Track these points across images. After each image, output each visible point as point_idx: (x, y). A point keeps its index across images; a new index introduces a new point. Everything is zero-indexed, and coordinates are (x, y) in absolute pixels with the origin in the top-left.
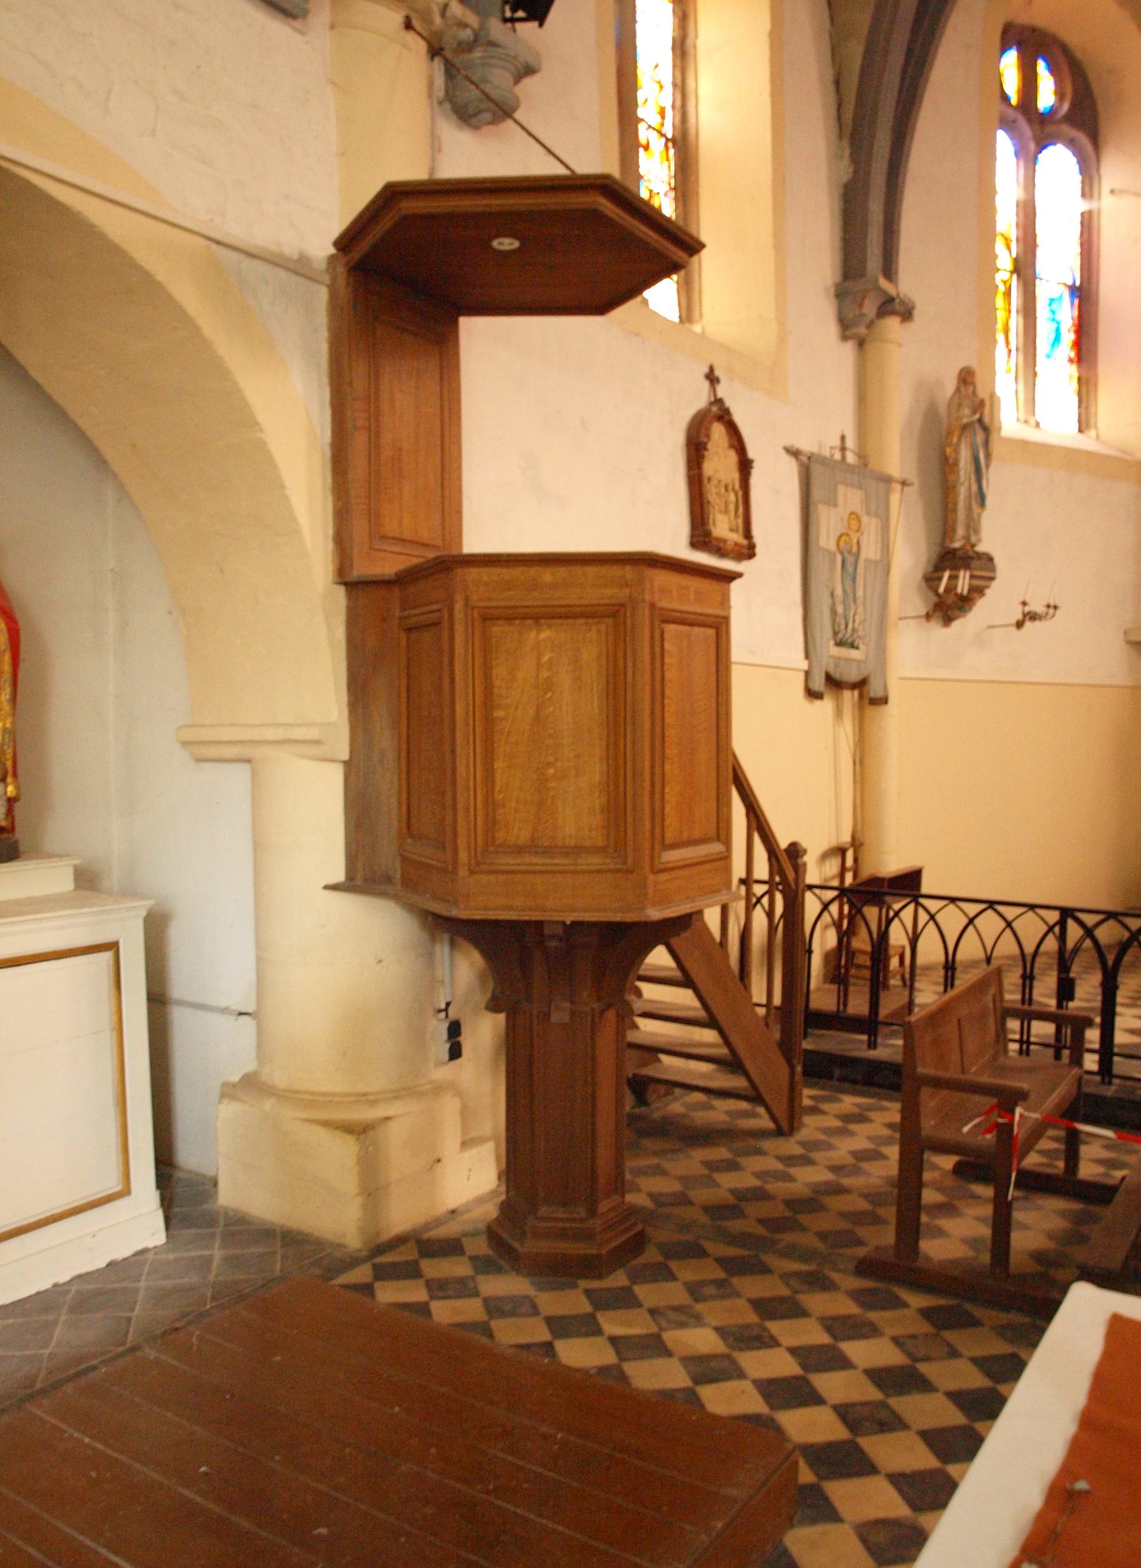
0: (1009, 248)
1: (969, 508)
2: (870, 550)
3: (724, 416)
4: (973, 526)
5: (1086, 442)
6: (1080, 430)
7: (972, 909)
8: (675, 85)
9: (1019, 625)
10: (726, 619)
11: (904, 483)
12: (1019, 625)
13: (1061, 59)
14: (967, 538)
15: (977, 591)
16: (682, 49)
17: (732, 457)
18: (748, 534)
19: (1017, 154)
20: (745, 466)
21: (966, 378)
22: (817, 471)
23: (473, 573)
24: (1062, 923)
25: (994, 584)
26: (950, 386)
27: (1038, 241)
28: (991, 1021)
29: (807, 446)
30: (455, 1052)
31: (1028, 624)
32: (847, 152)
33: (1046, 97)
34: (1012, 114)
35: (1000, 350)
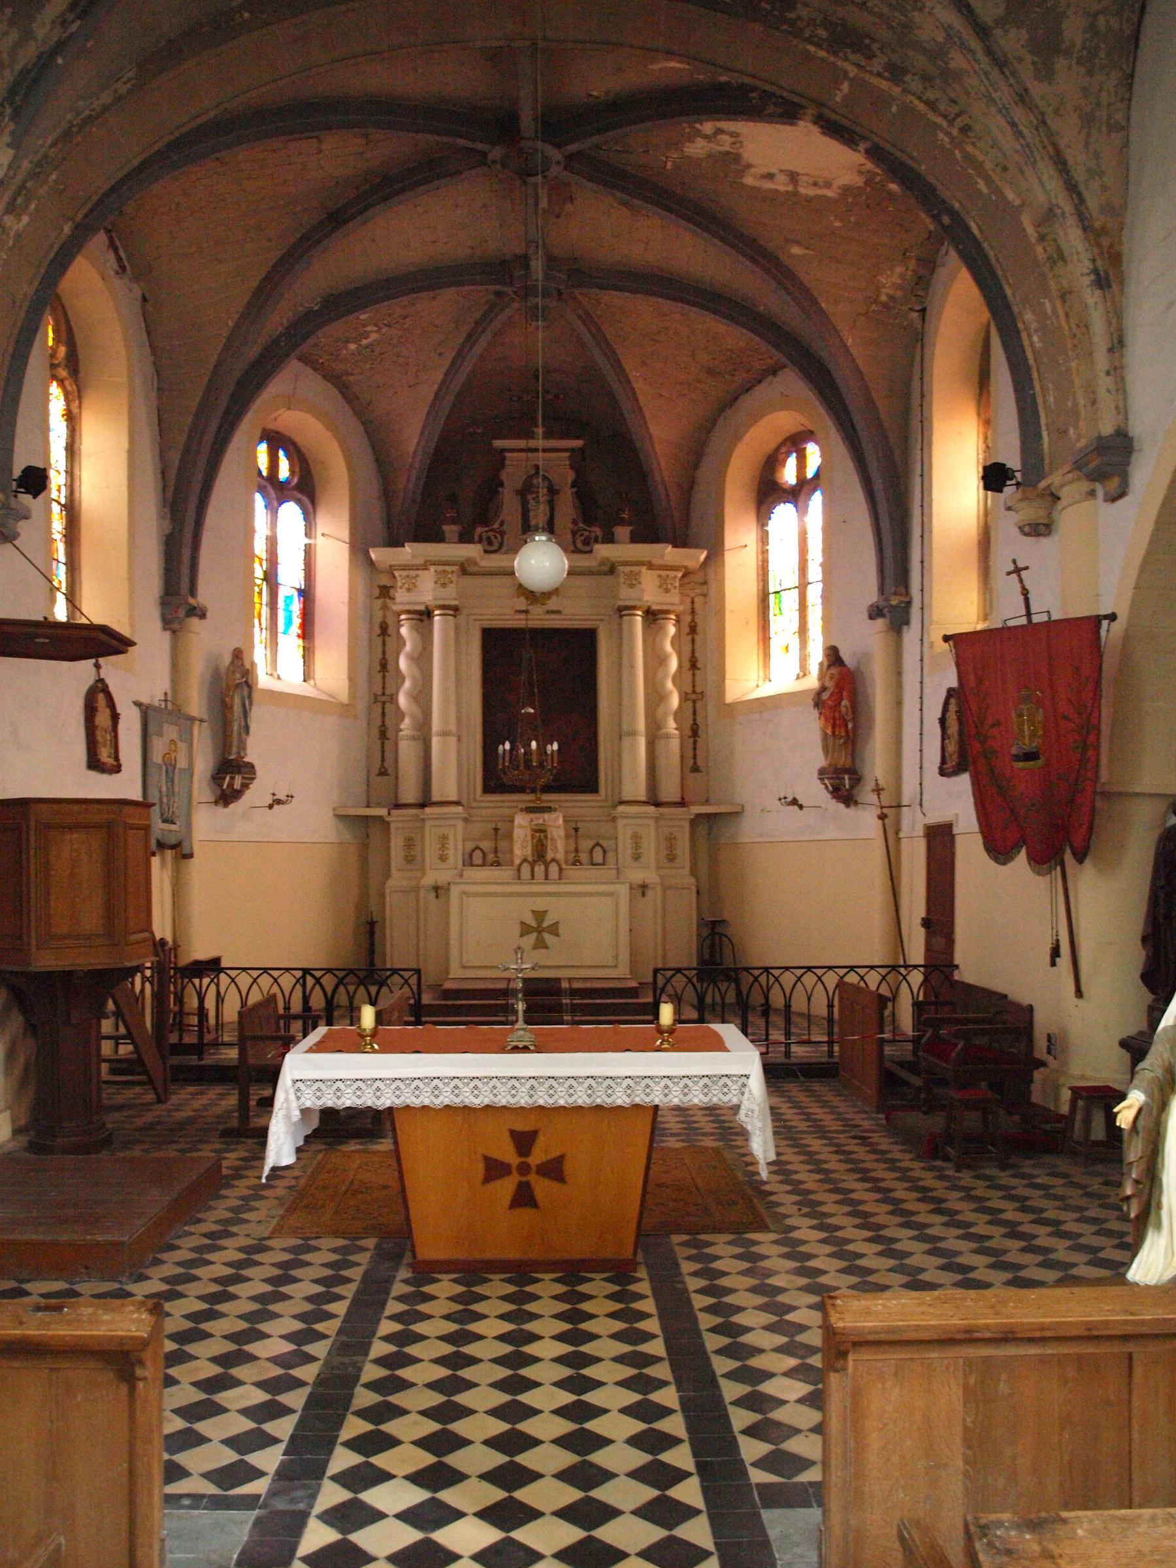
1: (240, 734)
2: (182, 763)
4: (242, 746)
5: (307, 690)
6: (305, 681)
8: (66, 472)
9: (271, 807)
10: (149, 826)
11: (201, 721)
12: (271, 807)
13: (291, 448)
14: (239, 753)
15: (245, 786)
16: (72, 450)
17: (108, 711)
18: (117, 759)
19: (266, 507)
21: (238, 654)
22: (150, 713)
24: (304, 977)
26: (227, 659)
27: (279, 561)
28: (273, 1021)
29: (145, 700)
32: (169, 516)
33: (284, 472)
34: (264, 483)
35: (256, 630)
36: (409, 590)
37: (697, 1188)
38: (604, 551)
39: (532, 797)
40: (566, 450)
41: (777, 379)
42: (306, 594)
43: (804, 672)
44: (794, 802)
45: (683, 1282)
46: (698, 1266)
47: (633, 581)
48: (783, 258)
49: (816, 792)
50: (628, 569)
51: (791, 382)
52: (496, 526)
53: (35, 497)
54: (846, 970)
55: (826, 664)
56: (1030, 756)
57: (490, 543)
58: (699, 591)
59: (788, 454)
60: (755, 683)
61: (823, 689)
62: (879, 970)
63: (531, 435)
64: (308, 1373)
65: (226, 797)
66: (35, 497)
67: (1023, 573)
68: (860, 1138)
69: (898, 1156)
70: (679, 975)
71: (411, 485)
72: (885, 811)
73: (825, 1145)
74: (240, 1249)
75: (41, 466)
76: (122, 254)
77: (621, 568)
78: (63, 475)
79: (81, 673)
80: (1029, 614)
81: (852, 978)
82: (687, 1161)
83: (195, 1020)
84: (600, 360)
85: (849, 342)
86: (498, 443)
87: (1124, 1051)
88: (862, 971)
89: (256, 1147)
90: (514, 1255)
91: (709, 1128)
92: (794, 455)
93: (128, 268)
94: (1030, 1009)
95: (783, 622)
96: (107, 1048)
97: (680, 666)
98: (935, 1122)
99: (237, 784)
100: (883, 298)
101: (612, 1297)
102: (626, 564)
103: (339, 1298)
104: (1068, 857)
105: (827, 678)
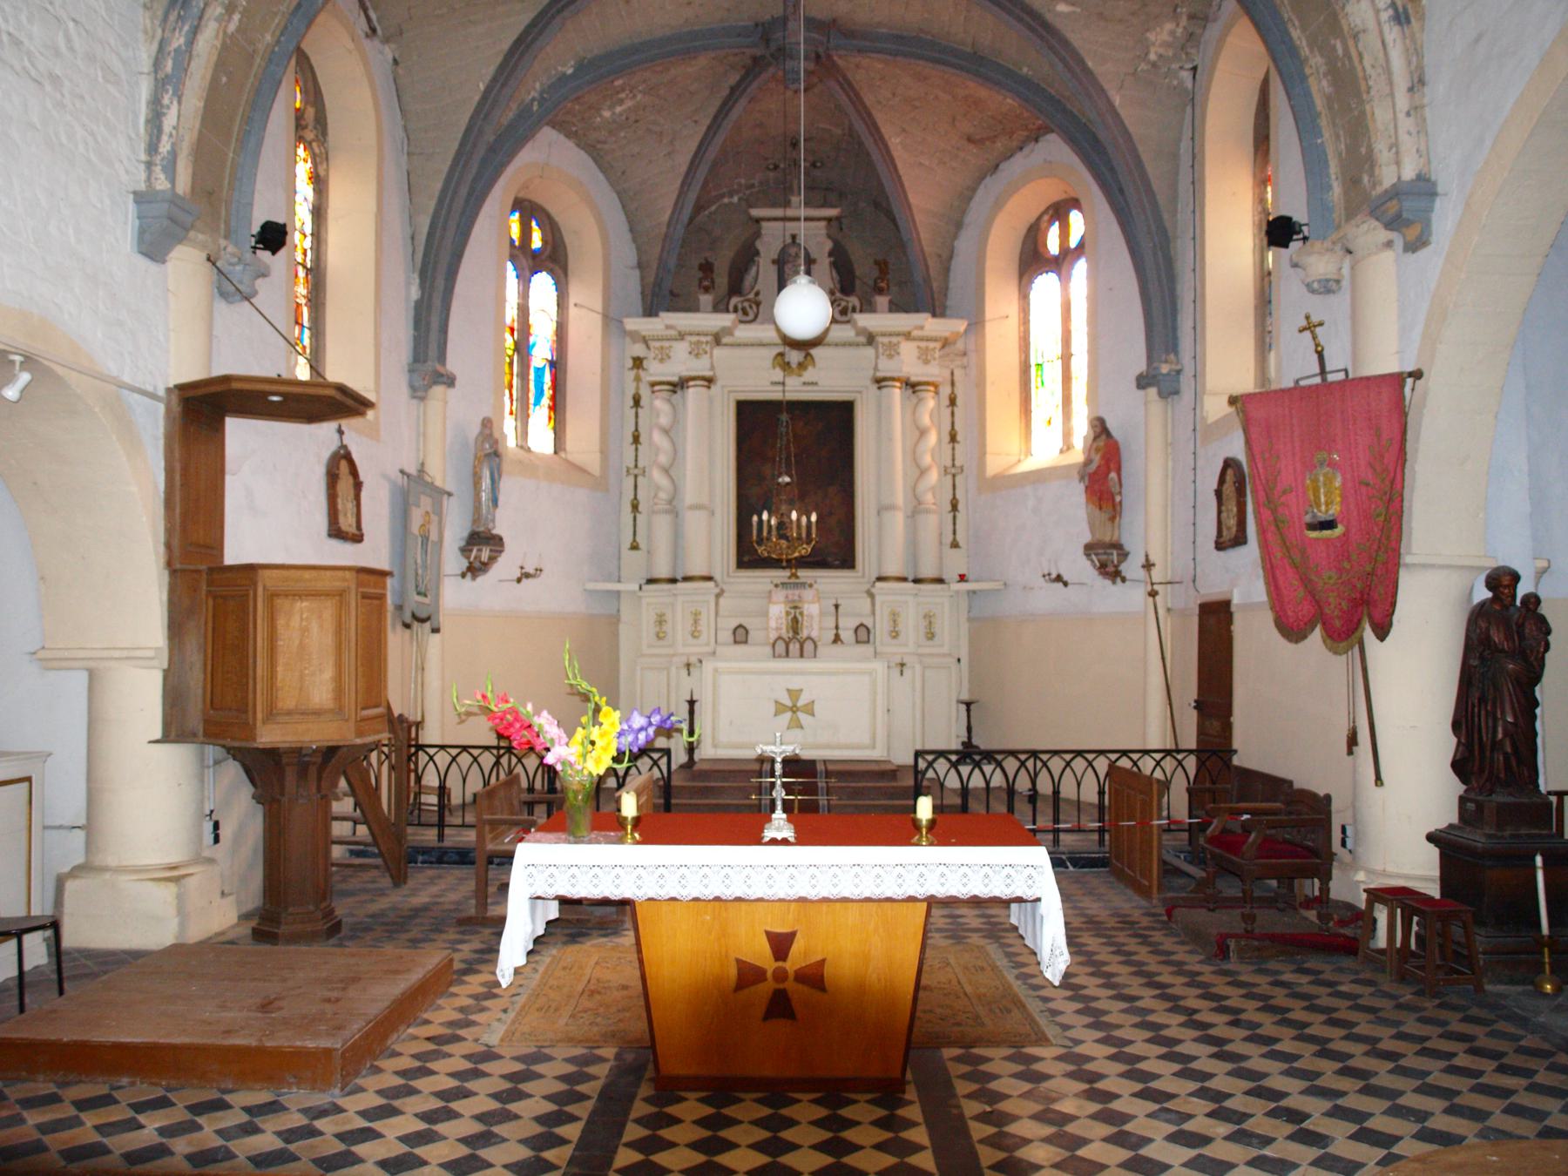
0: (512, 334)
2: (433, 537)
3: (348, 457)
7: (454, 752)
9: (519, 580)
12: (519, 580)
15: (492, 559)
16: (318, 213)
17: (351, 480)
20: (358, 486)
21: (487, 423)
23: (267, 573)
25: (503, 555)
30: (217, 840)
31: (524, 581)
33: (537, 242)
36: (662, 360)
37: (966, 994)
38: (865, 320)
39: (787, 573)
40: (819, 219)
41: (1040, 144)
42: (557, 366)
43: (1067, 447)
44: (1059, 578)
45: (959, 1107)
46: (974, 1087)
47: (892, 352)
48: (1049, 17)
49: (1081, 569)
50: (885, 340)
51: (1054, 148)
52: (751, 296)
53: (274, 253)
54: (458, 750)
55: (1092, 436)
56: (1329, 525)
57: (745, 313)
58: (958, 363)
59: (1051, 223)
60: (1016, 458)
61: (1088, 462)
62: (1154, 755)
63: (787, 204)
64: (590, 1088)
65: (475, 570)
66: (274, 253)
67: (1318, 330)
68: (1140, 936)
69: (1197, 968)
70: (465, 754)
71: (791, 916)
72: (1156, 587)
73: (1104, 944)
74: (468, 1057)
75: (281, 221)
76: (373, 16)
77: (880, 339)
78: (309, 239)
79: (321, 437)
80: (1323, 372)
81: (1125, 763)
82: (952, 961)
83: (434, 799)
84: (860, 127)
85: (1117, 101)
86: (755, 212)
87: (1432, 845)
88: (1135, 756)
89: (493, 937)
90: (768, 1072)
91: (976, 923)
92: (1057, 224)
93: (379, 31)
94: (1328, 798)
95: (1046, 398)
96: (340, 829)
97: (940, 440)
98: (1229, 920)
99: (485, 556)
100: (1152, 57)
101: (879, 1123)
102: (884, 335)
103: (573, 1118)
104: (1368, 634)
105: (1093, 452)
